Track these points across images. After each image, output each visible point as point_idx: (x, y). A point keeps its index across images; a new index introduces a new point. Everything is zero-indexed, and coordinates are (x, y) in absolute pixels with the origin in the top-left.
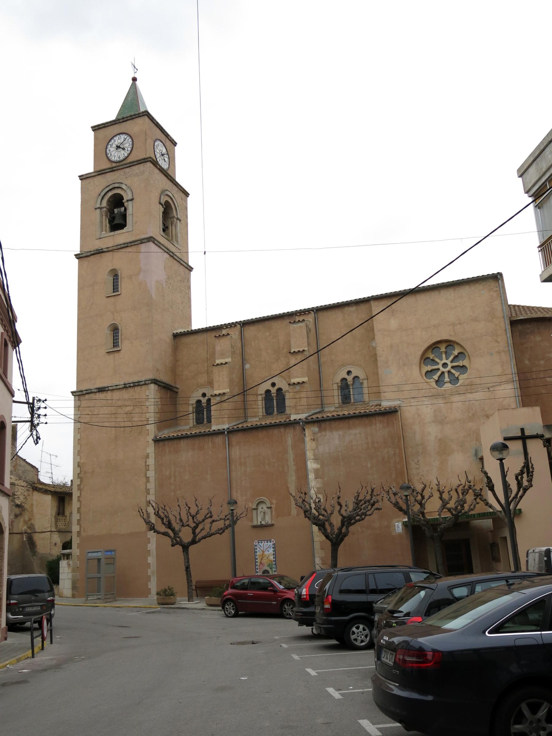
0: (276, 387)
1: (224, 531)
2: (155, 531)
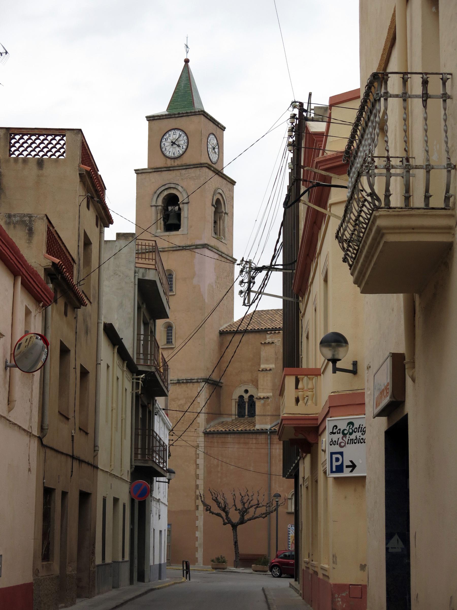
1: (266, 516)
2: (211, 512)
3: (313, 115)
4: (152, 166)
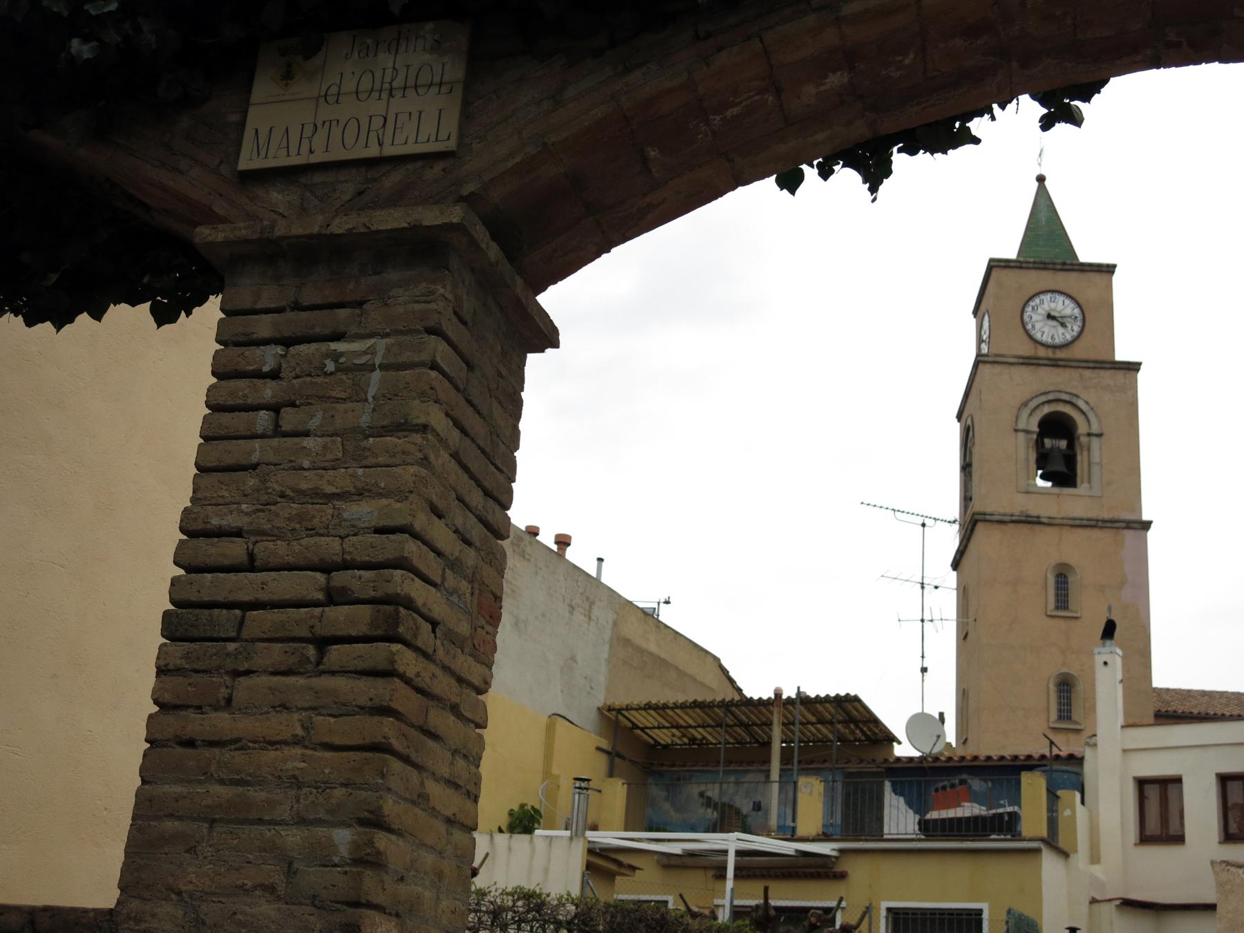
0: (1201, 809)
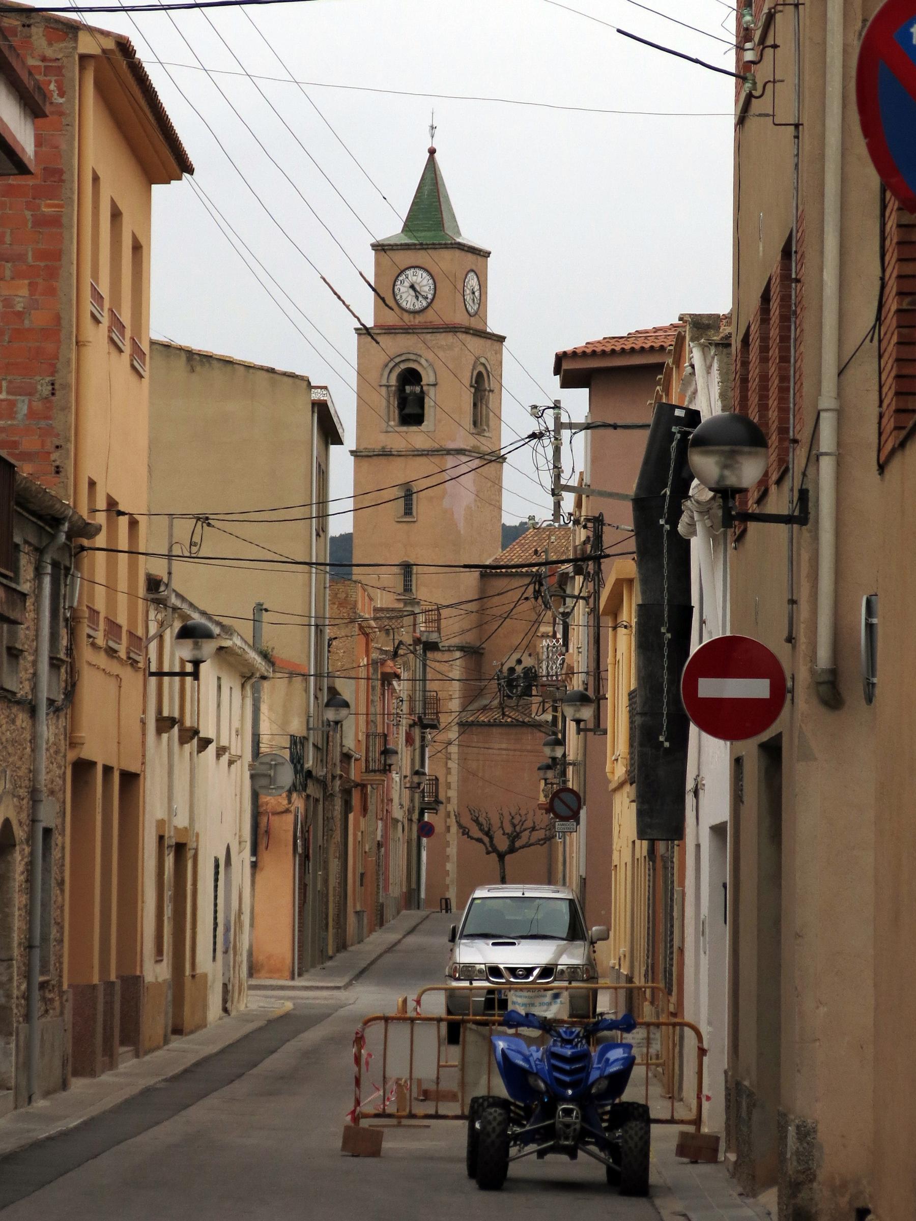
2: (469, 837)
3: (501, 1045)
4: (381, 322)
